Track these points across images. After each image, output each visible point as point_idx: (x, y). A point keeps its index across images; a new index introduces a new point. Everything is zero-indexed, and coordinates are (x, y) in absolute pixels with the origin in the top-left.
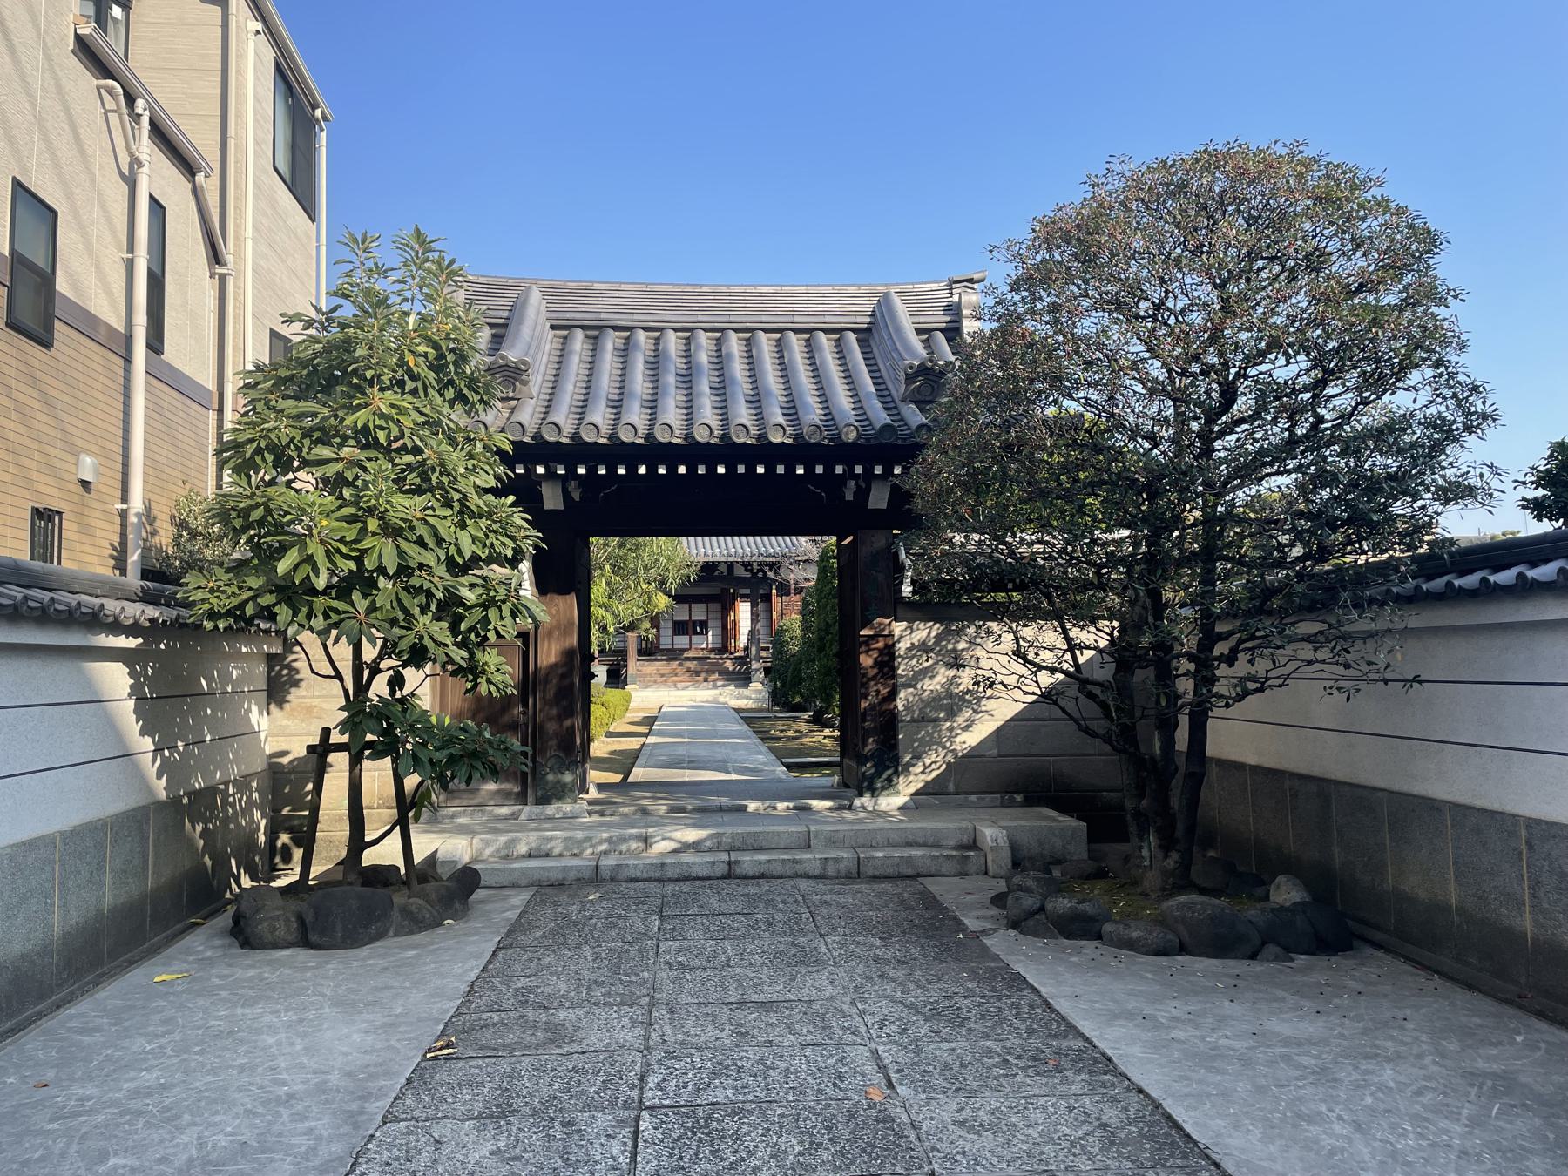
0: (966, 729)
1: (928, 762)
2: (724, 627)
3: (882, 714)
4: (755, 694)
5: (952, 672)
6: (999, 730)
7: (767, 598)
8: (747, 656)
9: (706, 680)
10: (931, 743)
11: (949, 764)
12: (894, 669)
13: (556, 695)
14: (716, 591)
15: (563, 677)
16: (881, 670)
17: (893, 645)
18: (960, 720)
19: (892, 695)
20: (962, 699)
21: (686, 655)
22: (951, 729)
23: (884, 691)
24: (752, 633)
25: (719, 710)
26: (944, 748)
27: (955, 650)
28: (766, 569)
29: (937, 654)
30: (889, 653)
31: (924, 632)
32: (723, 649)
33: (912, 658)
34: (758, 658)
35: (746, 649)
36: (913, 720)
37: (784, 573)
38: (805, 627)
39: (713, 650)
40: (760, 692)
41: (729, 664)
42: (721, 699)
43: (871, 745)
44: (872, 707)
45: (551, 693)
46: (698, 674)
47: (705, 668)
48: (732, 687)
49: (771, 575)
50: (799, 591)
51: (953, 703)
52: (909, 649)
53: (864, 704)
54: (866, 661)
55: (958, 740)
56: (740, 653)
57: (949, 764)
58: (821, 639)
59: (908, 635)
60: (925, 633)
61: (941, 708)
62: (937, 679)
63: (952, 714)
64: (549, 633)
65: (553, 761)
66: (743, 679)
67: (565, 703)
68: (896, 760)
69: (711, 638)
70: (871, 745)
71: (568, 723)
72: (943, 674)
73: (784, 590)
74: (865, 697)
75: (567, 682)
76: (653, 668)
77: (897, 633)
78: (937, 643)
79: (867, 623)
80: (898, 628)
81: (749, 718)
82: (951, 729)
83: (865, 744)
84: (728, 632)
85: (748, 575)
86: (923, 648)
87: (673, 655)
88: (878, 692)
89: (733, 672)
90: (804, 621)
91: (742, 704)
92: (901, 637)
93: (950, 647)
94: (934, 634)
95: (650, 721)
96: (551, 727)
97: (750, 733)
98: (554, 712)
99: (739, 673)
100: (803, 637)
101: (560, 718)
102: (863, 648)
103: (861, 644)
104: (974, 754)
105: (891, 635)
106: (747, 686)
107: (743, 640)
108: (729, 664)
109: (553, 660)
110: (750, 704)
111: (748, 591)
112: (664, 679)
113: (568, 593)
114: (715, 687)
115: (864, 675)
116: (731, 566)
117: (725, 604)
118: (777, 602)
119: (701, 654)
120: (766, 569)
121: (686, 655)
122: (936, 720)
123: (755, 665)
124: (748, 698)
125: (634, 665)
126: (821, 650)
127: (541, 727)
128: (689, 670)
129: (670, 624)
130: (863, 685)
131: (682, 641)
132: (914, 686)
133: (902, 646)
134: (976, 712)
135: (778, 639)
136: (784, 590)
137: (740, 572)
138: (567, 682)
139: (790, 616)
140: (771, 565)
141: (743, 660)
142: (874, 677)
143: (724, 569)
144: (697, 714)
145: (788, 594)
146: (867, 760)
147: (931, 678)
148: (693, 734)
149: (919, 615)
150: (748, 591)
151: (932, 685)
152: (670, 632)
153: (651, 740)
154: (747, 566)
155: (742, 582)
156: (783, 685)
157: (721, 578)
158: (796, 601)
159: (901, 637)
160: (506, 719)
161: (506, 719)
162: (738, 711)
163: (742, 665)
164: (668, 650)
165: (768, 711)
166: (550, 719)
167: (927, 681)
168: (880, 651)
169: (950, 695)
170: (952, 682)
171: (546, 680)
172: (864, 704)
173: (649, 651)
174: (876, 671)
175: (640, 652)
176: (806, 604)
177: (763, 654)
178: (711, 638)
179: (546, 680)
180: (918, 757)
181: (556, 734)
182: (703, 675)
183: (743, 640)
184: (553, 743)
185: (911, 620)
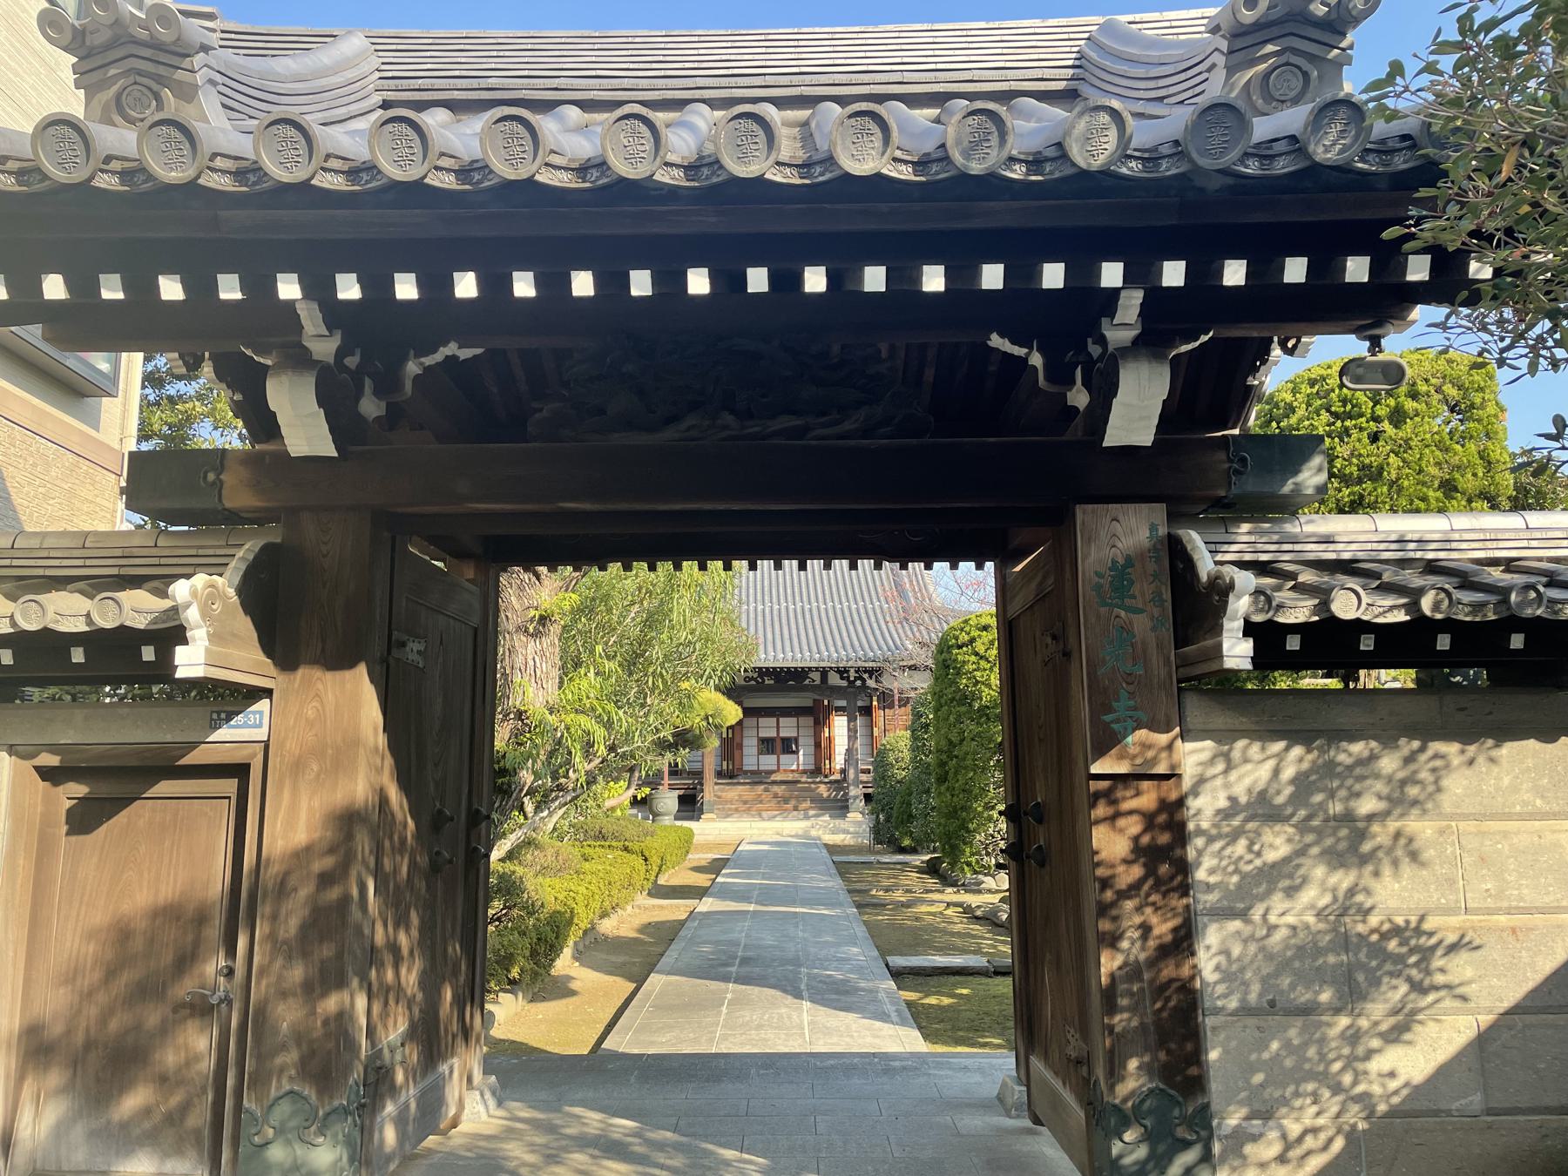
0: (1397, 1034)
1: (1294, 1129)
2: (818, 745)
3: (1160, 990)
4: (853, 827)
5: (1343, 880)
6: (1482, 1041)
7: (867, 711)
8: (845, 780)
9: (796, 808)
10: (1300, 1075)
11: (1352, 1136)
12: (1183, 868)
13: (304, 929)
14: (808, 703)
15: (326, 880)
16: (1150, 871)
17: (1181, 802)
18: (1377, 1010)
19: (1183, 941)
20: (1378, 951)
21: (774, 777)
22: (1353, 1037)
23: (1163, 928)
24: (849, 751)
25: (811, 843)
26: (1337, 1089)
27: (1348, 817)
28: (866, 676)
29: (1303, 827)
30: (1170, 823)
31: (1265, 765)
32: (817, 771)
33: (1234, 837)
34: (857, 782)
35: (843, 771)
36: (1245, 1010)
37: (887, 683)
38: (917, 747)
39: (804, 772)
40: (859, 823)
41: (823, 790)
42: (814, 833)
43: (1133, 1080)
44: (1132, 971)
45: (291, 926)
46: (786, 801)
47: (792, 796)
48: (827, 818)
49: (871, 683)
50: (904, 702)
51: (1369, 963)
52: (1225, 814)
53: (1109, 963)
54: (1111, 843)
55: (1376, 1065)
56: (837, 777)
57: (1352, 1136)
58: (942, 764)
59: (1220, 774)
60: (1264, 772)
61: (1321, 977)
62: (1308, 895)
63: (1352, 994)
64: (298, 767)
65: (284, 1108)
66: (840, 807)
67: (327, 951)
68: (1202, 1122)
69: (803, 758)
70: (1133, 1080)
71: (331, 1003)
72: (1321, 887)
73: (886, 700)
74: (1112, 940)
75: (334, 894)
76: (734, 792)
77: (1189, 771)
78: (1295, 800)
79: (1106, 742)
80: (1193, 756)
81: (843, 862)
82: (1353, 1037)
83: (1115, 1073)
84: (822, 750)
85: (844, 683)
86: (1263, 810)
87: (759, 777)
88: (1146, 929)
89: (828, 800)
90: (915, 738)
91: (838, 839)
92: (1201, 781)
93: (1336, 808)
94: (1288, 773)
95: (716, 867)
96: (287, 1016)
97: (844, 897)
98: (297, 973)
99: (835, 800)
100: (913, 760)
101: (315, 988)
102: (1101, 810)
103: (1095, 798)
104: (1421, 1107)
105: (1172, 776)
106: (844, 816)
107: (839, 761)
108: (823, 790)
109: (301, 836)
110: (848, 840)
111: (843, 703)
112: (748, 808)
113: (350, 664)
114: (807, 817)
115: (1105, 883)
116: (824, 673)
117: (818, 716)
118: (879, 715)
119: (790, 777)
120: (866, 676)
121: (774, 777)
122: (1307, 1010)
123: (853, 791)
124: (846, 832)
125: (711, 791)
126: (942, 779)
127: (261, 1012)
128: (776, 796)
129: (755, 741)
130: (1103, 910)
131: (768, 761)
132: (1243, 915)
133: (1204, 808)
134: (1419, 988)
135: (881, 761)
136: (886, 700)
137: (834, 679)
138: (334, 894)
139: (895, 733)
140: (871, 672)
141: (840, 785)
142: (1135, 888)
143: (816, 676)
144: (780, 858)
145: (891, 706)
146: (1125, 1122)
147: (1291, 892)
148: (766, 896)
149: (1242, 722)
150: (843, 703)
151: (1294, 912)
152: (755, 750)
153: (706, 905)
154: (843, 672)
155: (837, 691)
156: (887, 820)
157: (813, 688)
158: (902, 716)
159: (1201, 781)
160: (185, 988)
161: (185, 988)
162: (832, 849)
163: (838, 790)
164: (753, 772)
165: (871, 851)
166: (284, 995)
167: (1278, 902)
168: (1149, 819)
169: (1345, 942)
170: (1347, 906)
171: (282, 889)
172: (1109, 963)
173: (729, 774)
174: (1137, 871)
175: (719, 774)
176: (918, 716)
177: (864, 777)
178: (803, 758)
179: (282, 889)
180: (1265, 1114)
181: (299, 1037)
182: (793, 802)
183: (839, 761)
184: (291, 1057)
185: (1225, 736)
